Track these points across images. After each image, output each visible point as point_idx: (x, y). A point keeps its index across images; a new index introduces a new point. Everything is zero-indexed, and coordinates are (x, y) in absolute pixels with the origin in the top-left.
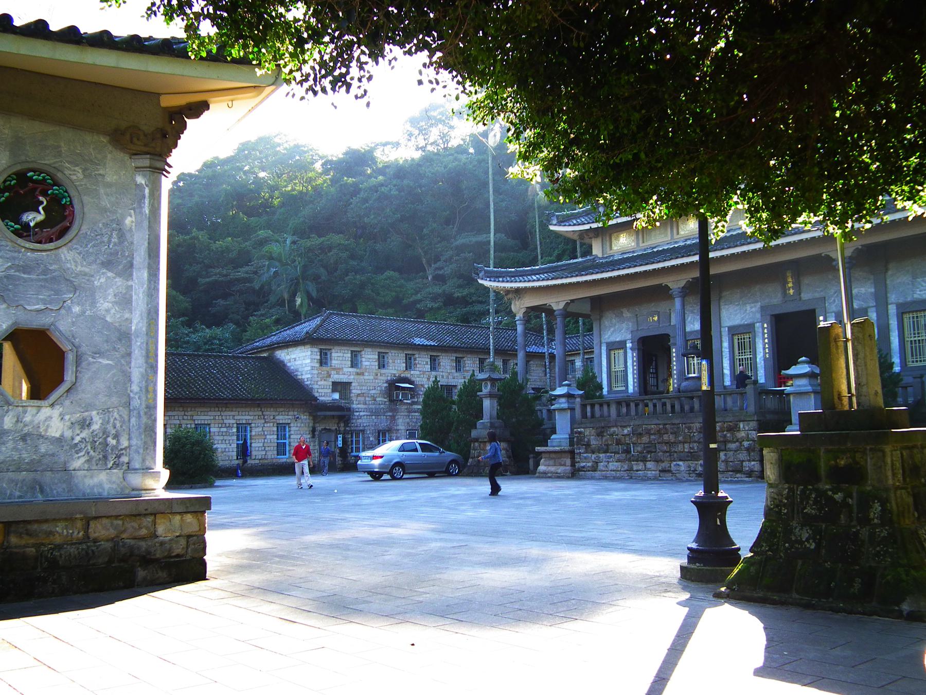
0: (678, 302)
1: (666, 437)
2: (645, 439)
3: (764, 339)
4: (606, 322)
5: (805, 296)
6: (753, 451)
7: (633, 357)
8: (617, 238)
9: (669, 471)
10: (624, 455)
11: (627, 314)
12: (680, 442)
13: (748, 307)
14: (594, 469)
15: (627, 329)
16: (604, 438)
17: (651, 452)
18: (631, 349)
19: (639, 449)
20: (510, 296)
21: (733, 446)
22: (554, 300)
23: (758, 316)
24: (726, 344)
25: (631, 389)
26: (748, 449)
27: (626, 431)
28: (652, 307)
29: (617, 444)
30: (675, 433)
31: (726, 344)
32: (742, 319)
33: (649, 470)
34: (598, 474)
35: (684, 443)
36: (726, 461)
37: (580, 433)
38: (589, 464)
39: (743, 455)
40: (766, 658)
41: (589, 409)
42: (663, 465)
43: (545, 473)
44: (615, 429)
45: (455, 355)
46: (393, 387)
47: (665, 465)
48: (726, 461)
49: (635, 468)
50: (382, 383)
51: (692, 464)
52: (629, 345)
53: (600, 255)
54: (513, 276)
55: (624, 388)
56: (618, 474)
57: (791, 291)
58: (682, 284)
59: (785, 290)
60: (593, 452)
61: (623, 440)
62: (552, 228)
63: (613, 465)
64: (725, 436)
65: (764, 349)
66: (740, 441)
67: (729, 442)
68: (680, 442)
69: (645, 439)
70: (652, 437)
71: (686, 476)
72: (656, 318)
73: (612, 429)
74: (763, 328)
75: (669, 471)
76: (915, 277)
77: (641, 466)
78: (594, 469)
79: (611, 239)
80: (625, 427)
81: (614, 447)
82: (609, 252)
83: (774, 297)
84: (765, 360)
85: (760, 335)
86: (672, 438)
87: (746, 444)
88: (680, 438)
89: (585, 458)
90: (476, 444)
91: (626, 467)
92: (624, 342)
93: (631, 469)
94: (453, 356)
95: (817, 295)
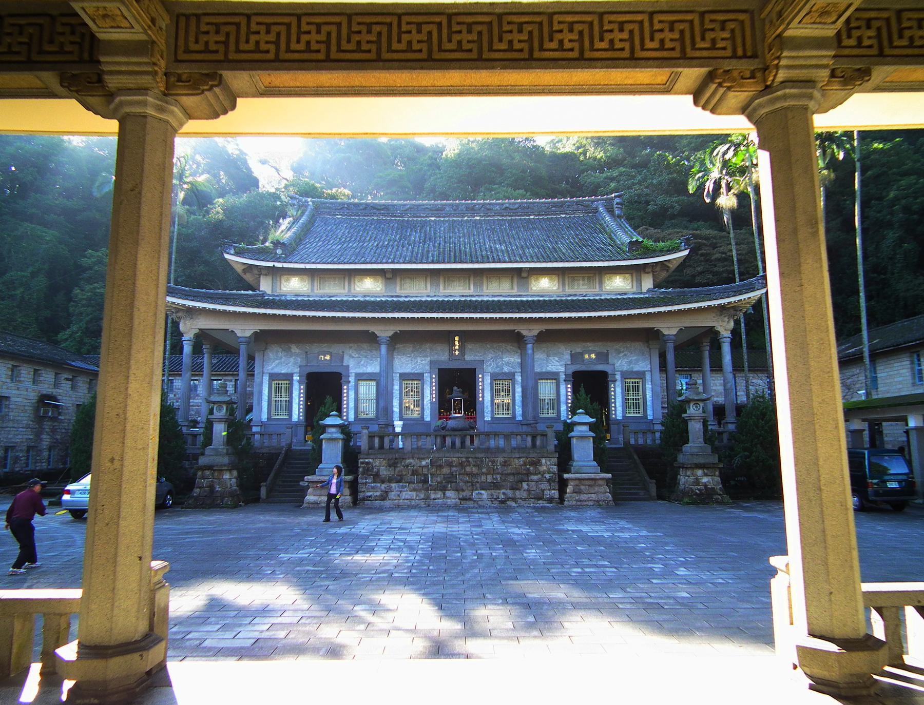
0: (384, 348)
1: (468, 469)
2: (446, 470)
3: (431, 387)
4: (271, 354)
5: (468, 357)
6: (554, 481)
7: (300, 389)
8: (288, 280)
9: (471, 499)
10: (421, 485)
11: (295, 349)
12: (483, 474)
13: (419, 360)
14: (384, 497)
15: (295, 363)
16: (397, 469)
17: (451, 482)
18: (300, 382)
19: (439, 479)
20: (180, 314)
21: (535, 477)
22: (239, 327)
23: (428, 368)
24: (396, 387)
25: (295, 417)
26: (549, 481)
27: (424, 463)
28: (324, 347)
29: (413, 474)
30: (479, 466)
31: (396, 387)
32: (413, 368)
33: (448, 498)
34: (387, 503)
35: (487, 474)
36: (528, 491)
37: (368, 463)
38: (378, 494)
39: (544, 486)
40: (35, 700)
41: (377, 440)
42: (464, 494)
43: (570, 506)
44: (411, 461)
45: (12, 363)
46: (44, 400)
47: (466, 494)
48: (528, 491)
49: (433, 496)
50: (33, 396)
51: (495, 493)
52: (296, 378)
53: (269, 292)
54: (186, 296)
55: (287, 417)
56: (413, 503)
57: (457, 353)
58: (390, 333)
59: (451, 350)
60: (383, 482)
61: (420, 471)
62: (227, 256)
63: (407, 494)
64: (529, 469)
65: (431, 394)
66: (542, 474)
67: (532, 474)
68: (483, 474)
69: (446, 470)
70: (454, 469)
71: (489, 503)
72: (328, 357)
73: (408, 461)
74: (431, 378)
75: (471, 499)
76: (548, 356)
77: (439, 494)
78: (384, 496)
79: (918, 356)
80: (424, 459)
81: (409, 477)
82: (278, 292)
83: (441, 355)
84: (432, 403)
85: (429, 383)
86: (475, 470)
87: (548, 476)
88: (484, 470)
89: (373, 488)
90: (207, 472)
91: (422, 496)
92: (292, 375)
93: (427, 498)
94: (10, 364)
95: (477, 358)
